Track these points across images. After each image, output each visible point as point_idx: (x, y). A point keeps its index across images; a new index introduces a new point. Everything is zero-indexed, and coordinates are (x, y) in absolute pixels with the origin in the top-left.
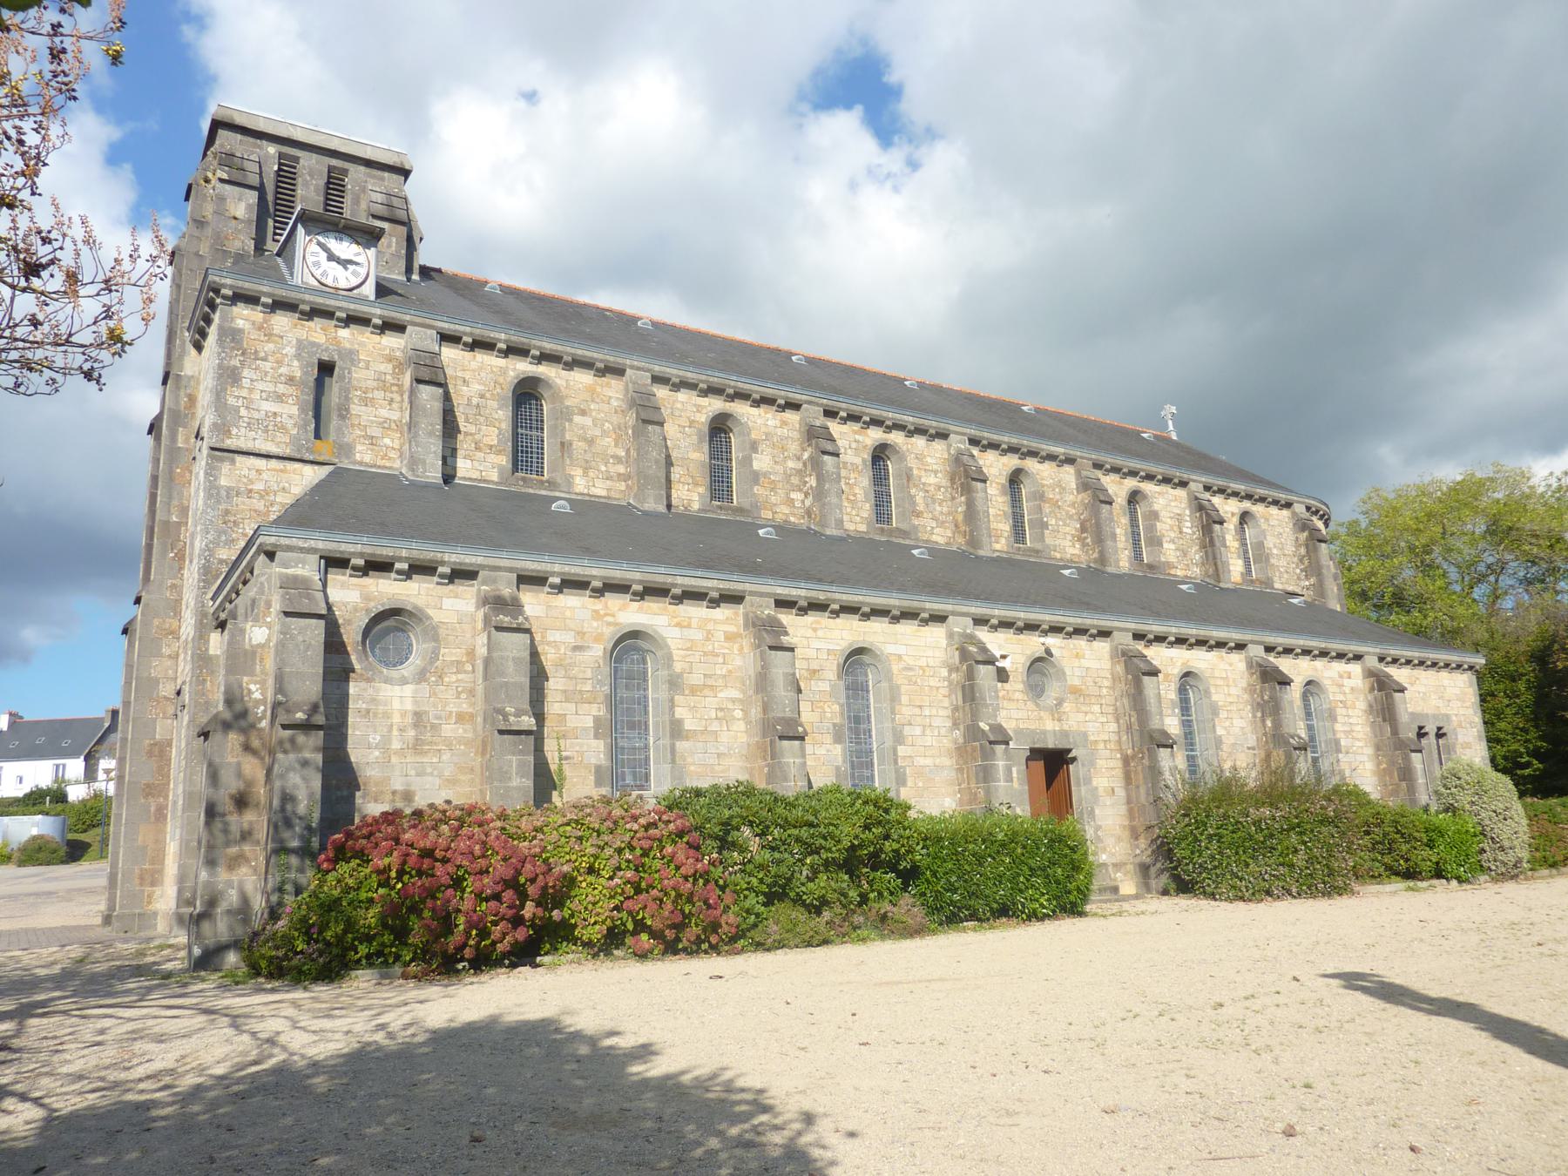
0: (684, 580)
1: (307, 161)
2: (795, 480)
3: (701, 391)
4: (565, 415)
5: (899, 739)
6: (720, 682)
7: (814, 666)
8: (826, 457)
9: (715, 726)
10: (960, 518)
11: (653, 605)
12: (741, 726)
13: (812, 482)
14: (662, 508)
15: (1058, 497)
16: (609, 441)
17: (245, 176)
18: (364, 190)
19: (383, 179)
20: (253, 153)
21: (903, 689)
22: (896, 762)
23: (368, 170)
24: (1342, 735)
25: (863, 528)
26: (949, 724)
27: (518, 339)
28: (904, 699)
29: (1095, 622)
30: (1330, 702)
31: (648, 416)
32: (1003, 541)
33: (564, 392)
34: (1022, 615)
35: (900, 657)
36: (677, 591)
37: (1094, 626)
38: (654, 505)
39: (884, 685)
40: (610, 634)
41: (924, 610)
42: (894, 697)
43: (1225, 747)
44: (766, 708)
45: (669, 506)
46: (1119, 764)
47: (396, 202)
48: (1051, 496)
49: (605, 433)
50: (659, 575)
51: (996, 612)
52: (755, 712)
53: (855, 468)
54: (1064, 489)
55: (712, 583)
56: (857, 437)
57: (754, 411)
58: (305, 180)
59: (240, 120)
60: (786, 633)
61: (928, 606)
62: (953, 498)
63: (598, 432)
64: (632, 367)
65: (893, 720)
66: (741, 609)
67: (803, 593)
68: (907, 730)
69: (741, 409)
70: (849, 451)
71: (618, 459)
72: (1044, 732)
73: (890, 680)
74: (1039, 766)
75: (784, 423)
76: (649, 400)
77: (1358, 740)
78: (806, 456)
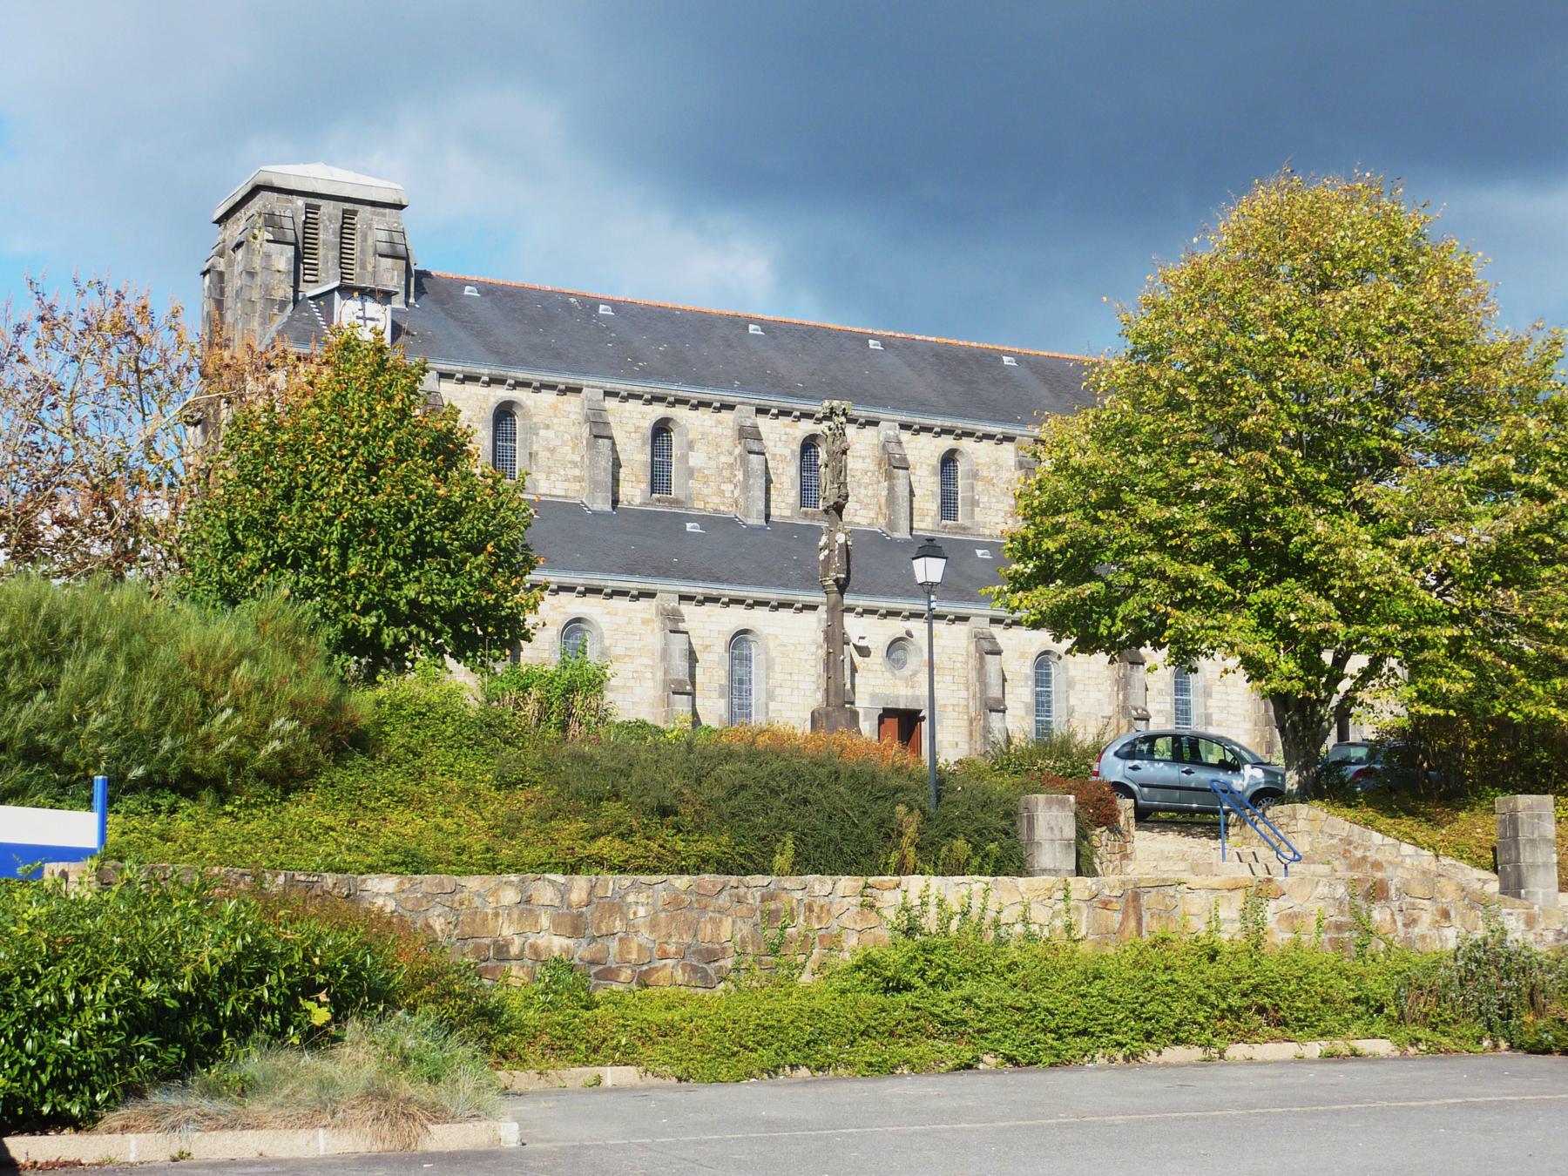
0: (612, 582)
1: (327, 208)
2: (726, 473)
3: (646, 400)
4: (533, 430)
5: (771, 696)
6: (636, 653)
7: (707, 642)
8: (752, 456)
9: (631, 683)
10: (883, 501)
11: (592, 600)
12: (650, 683)
13: (740, 476)
14: (608, 507)
15: (993, 475)
16: (568, 449)
17: (284, 233)
18: (370, 227)
19: (384, 215)
20: (287, 208)
21: (777, 660)
22: (767, 713)
23: (374, 209)
24: (1217, 710)
25: (788, 513)
26: (814, 687)
27: (498, 372)
28: (778, 668)
29: (953, 610)
30: (1206, 680)
31: (599, 430)
32: (929, 519)
33: (533, 411)
34: (884, 604)
35: (776, 636)
36: (609, 591)
37: (951, 613)
38: (602, 504)
39: (763, 657)
40: (562, 620)
41: (798, 602)
42: (769, 666)
43: (1076, 715)
44: (666, 672)
45: (615, 502)
46: (966, 723)
47: (397, 238)
48: (986, 474)
49: (564, 443)
50: (596, 579)
51: (861, 603)
52: (660, 675)
53: (783, 459)
54: (1001, 467)
55: (634, 584)
56: (788, 430)
57: (694, 413)
58: (326, 226)
59: (278, 183)
60: (683, 621)
61: (800, 598)
62: (879, 482)
63: (558, 442)
64: (588, 386)
65: (767, 683)
66: (654, 602)
67: (700, 590)
68: (778, 691)
69: (680, 413)
70: (779, 444)
71: (575, 464)
72: (897, 697)
73: (767, 653)
74: (893, 723)
75: (719, 422)
76: (600, 415)
77: (1235, 715)
78: (737, 452)
